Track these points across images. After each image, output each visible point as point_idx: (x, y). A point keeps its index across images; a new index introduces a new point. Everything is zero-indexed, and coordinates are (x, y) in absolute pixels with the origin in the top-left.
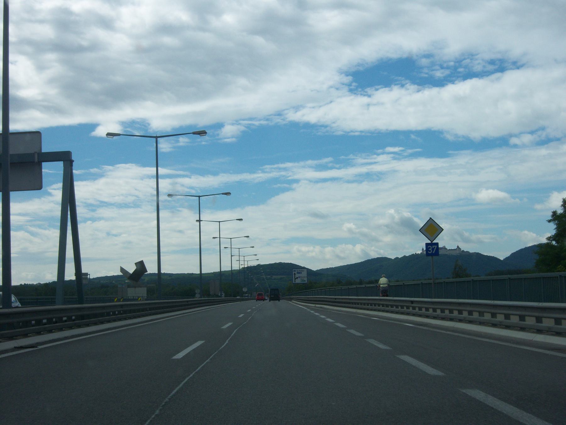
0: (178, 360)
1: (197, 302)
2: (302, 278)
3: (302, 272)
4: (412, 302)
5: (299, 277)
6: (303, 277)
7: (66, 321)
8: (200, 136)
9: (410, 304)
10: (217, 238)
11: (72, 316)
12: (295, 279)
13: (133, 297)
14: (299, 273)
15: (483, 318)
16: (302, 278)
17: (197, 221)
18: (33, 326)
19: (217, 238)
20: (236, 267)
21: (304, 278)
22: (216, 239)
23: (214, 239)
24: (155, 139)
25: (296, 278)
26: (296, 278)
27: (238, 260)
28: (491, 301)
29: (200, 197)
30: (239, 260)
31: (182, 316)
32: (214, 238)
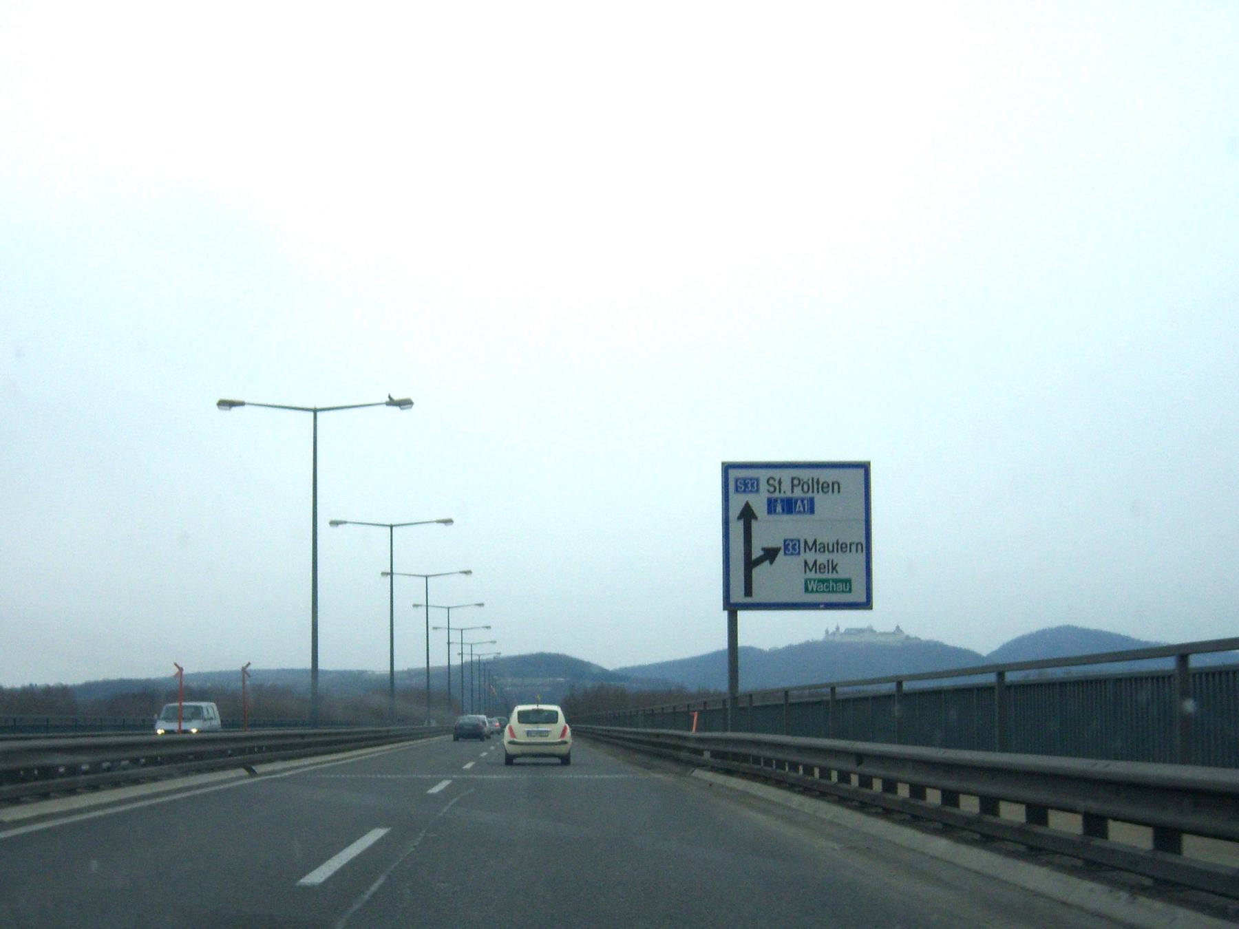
0: (432, 794)
1: (319, 739)
2: (822, 558)
3: (820, 499)
4: (860, 757)
5: (791, 547)
6: (824, 548)
7: (109, 769)
8: (401, 409)
9: (848, 765)
10: (421, 605)
11: (33, 769)
12: (750, 564)
13: (15, 720)
14: (789, 506)
15: (699, 757)
16: (822, 558)
17: (459, 654)
18: (62, 776)
19: (421, 605)
20: (456, 661)
21: (838, 557)
22: (340, 526)
23: (415, 608)
24: (312, 414)
25: (757, 553)
26: (757, 553)
27: (387, 574)
28: (1093, 761)
29: (319, 414)
30: (391, 574)
31: (151, 807)
32: (416, 606)
